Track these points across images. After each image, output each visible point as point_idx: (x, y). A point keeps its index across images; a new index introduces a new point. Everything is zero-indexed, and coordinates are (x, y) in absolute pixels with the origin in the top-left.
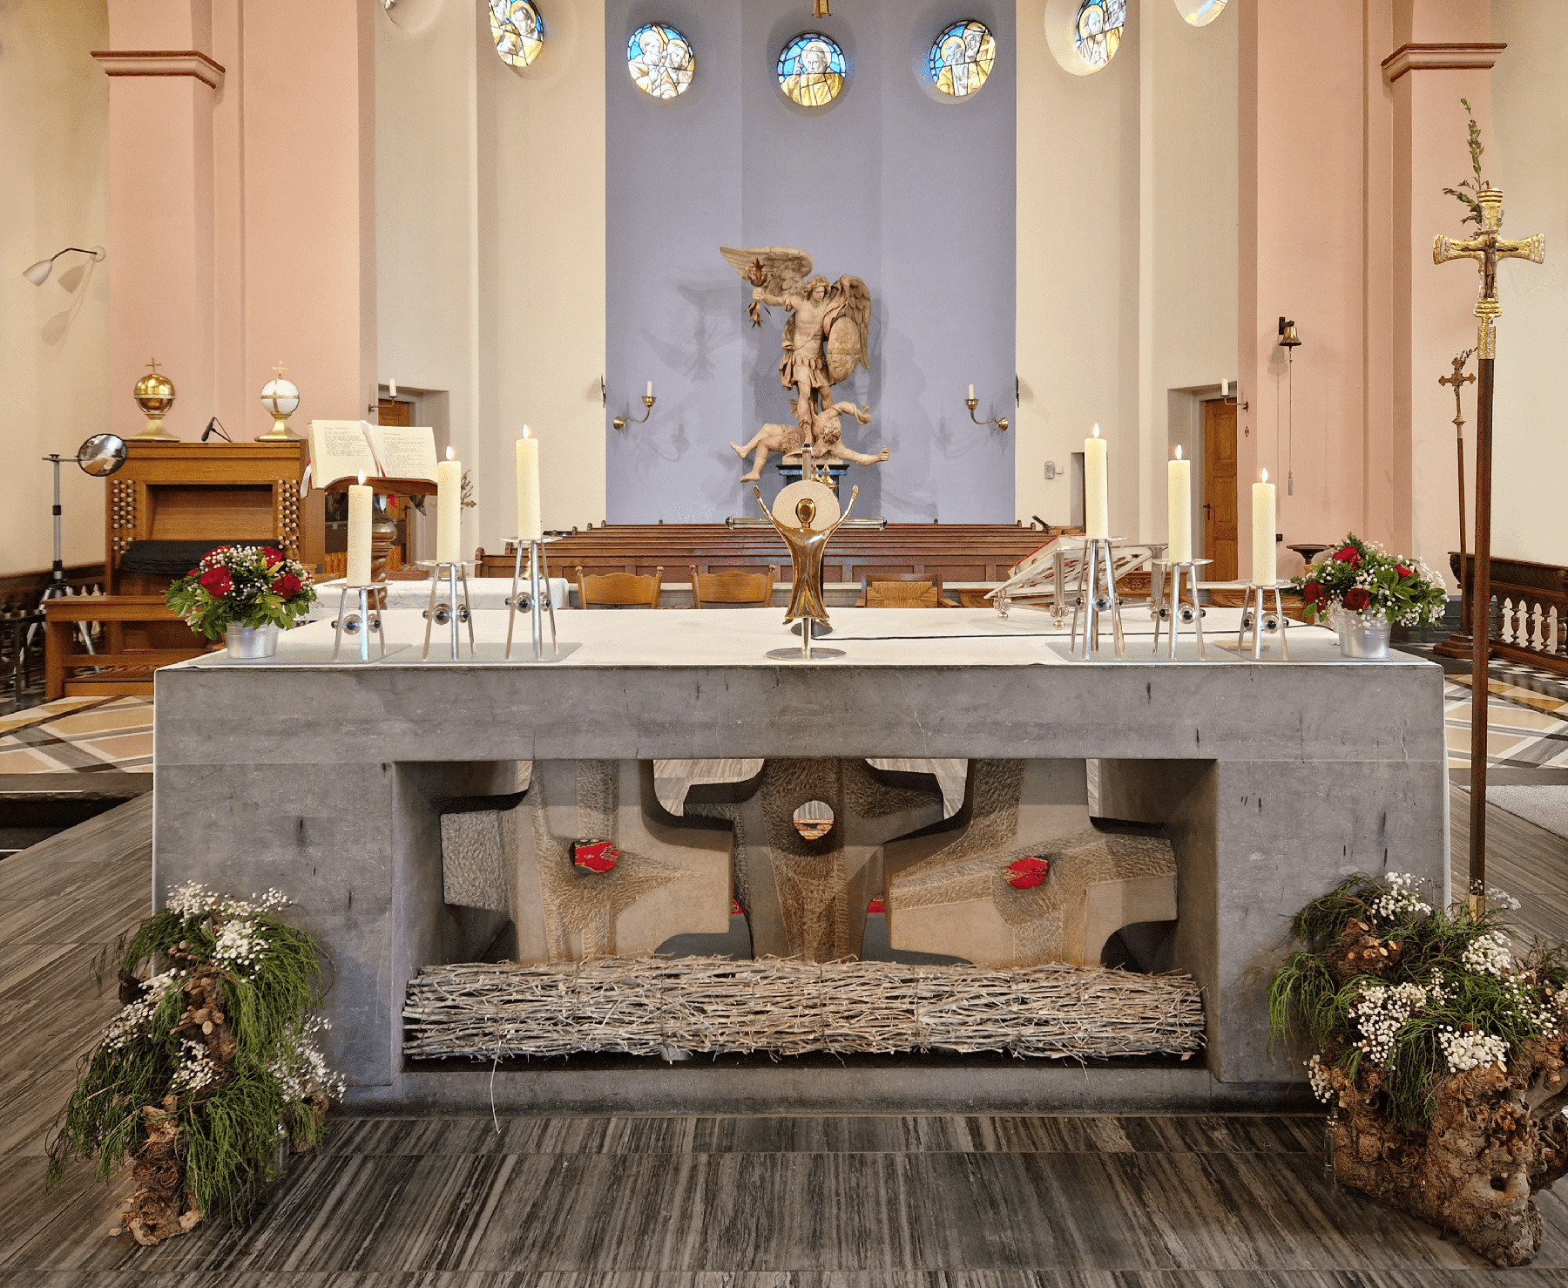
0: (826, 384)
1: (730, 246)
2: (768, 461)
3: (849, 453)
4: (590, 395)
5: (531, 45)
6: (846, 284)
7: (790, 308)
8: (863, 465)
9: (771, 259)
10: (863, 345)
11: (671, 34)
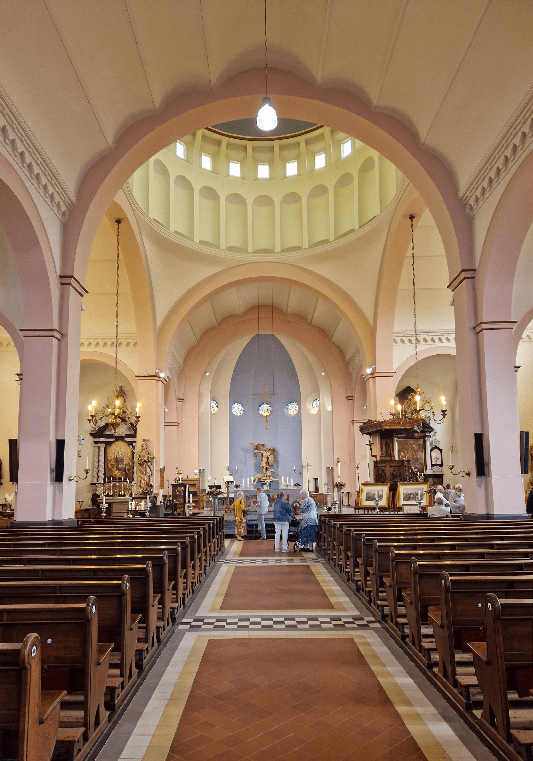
0: (268, 466)
1: (251, 443)
2: (258, 480)
3: (273, 479)
4: (226, 469)
5: (216, 409)
6: (272, 449)
7: (262, 453)
8: (275, 481)
9: (258, 445)
10: (275, 460)
11: (240, 404)
